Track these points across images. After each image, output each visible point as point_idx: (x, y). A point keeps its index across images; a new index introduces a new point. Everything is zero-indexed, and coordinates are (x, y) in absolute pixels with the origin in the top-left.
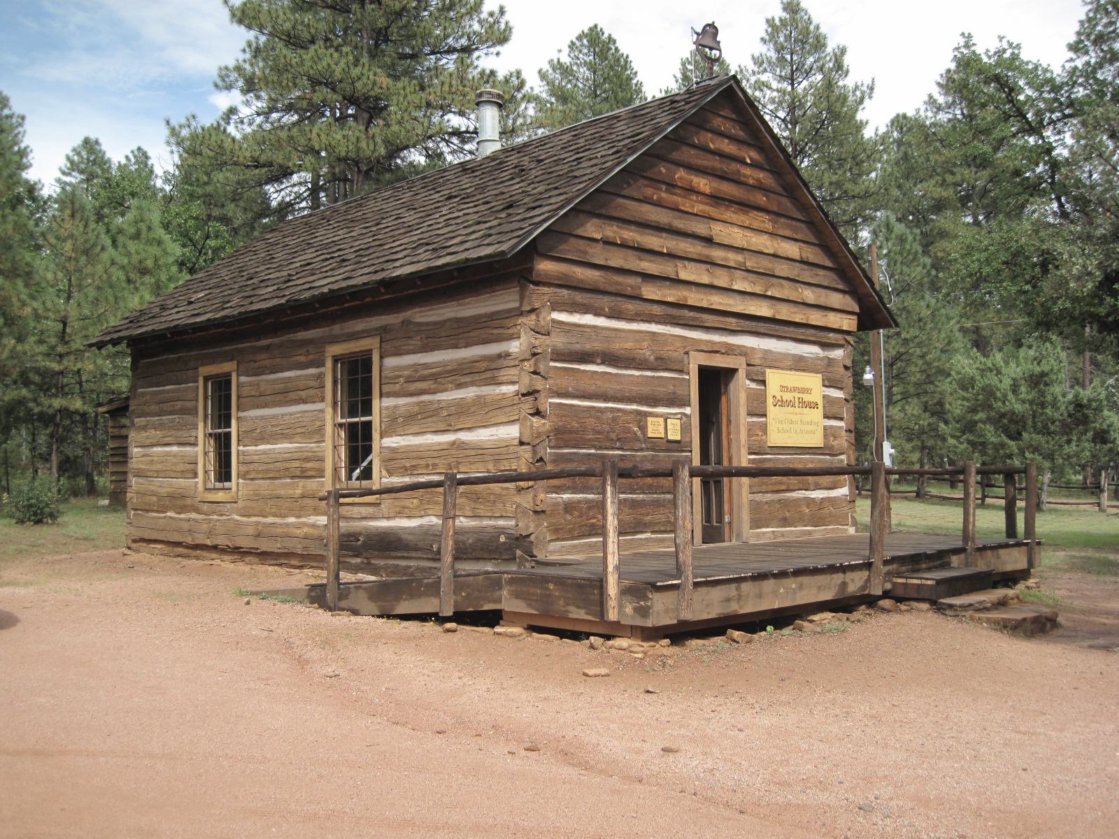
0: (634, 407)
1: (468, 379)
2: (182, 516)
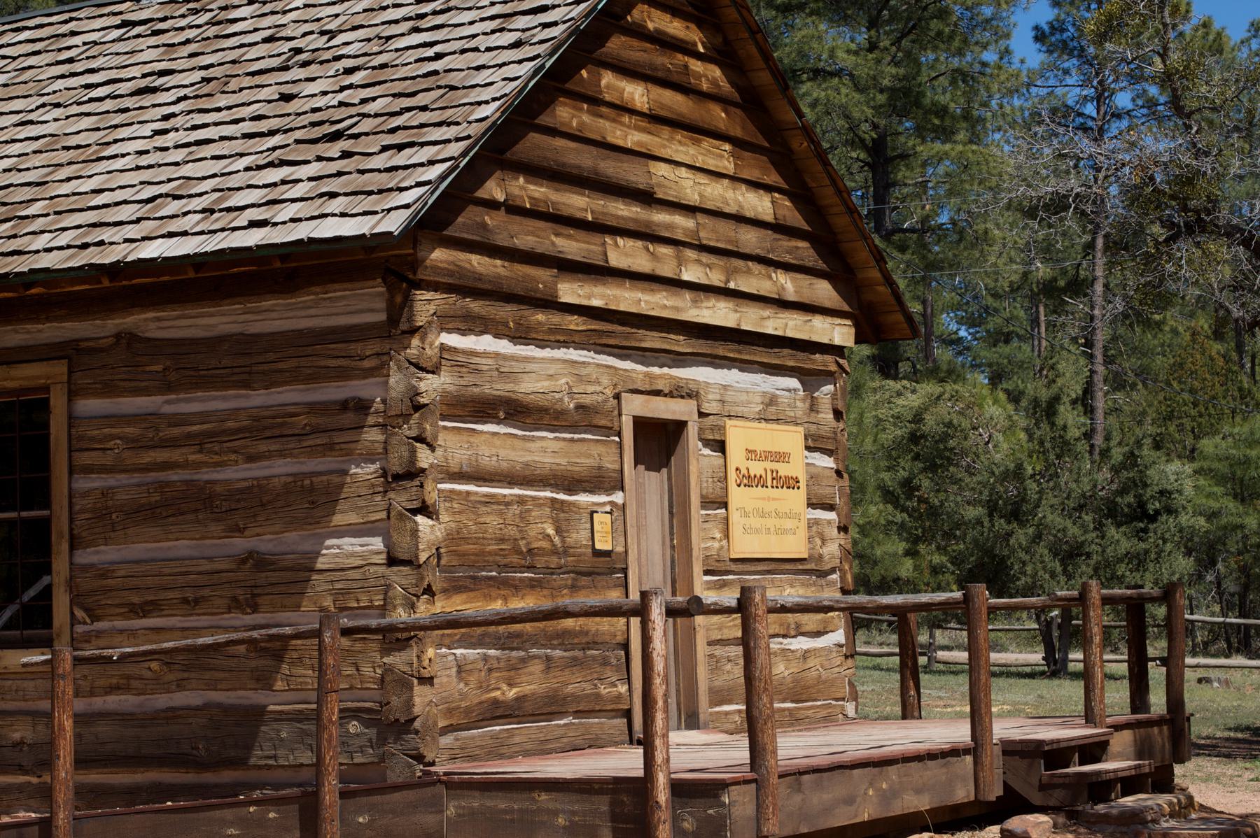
0: (548, 494)
1: (274, 446)
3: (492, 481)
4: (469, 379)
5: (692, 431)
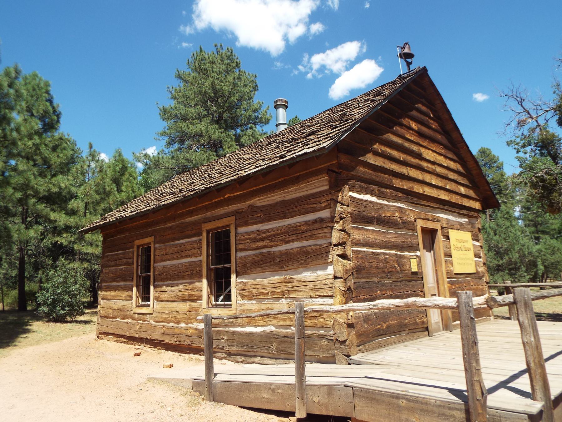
0: (382, 251)
2: (124, 321)
3: (373, 247)
4: (363, 209)
5: (439, 232)
